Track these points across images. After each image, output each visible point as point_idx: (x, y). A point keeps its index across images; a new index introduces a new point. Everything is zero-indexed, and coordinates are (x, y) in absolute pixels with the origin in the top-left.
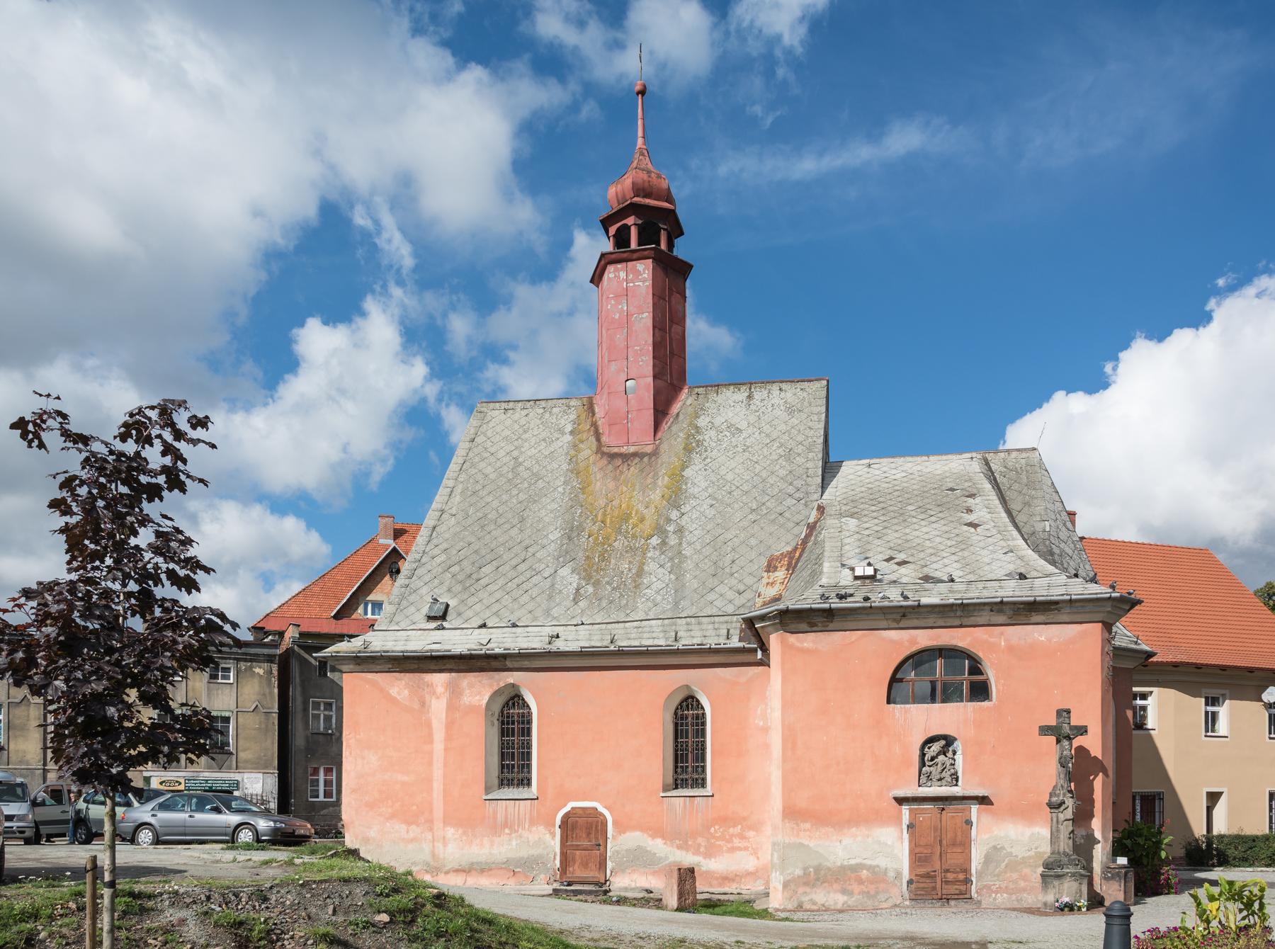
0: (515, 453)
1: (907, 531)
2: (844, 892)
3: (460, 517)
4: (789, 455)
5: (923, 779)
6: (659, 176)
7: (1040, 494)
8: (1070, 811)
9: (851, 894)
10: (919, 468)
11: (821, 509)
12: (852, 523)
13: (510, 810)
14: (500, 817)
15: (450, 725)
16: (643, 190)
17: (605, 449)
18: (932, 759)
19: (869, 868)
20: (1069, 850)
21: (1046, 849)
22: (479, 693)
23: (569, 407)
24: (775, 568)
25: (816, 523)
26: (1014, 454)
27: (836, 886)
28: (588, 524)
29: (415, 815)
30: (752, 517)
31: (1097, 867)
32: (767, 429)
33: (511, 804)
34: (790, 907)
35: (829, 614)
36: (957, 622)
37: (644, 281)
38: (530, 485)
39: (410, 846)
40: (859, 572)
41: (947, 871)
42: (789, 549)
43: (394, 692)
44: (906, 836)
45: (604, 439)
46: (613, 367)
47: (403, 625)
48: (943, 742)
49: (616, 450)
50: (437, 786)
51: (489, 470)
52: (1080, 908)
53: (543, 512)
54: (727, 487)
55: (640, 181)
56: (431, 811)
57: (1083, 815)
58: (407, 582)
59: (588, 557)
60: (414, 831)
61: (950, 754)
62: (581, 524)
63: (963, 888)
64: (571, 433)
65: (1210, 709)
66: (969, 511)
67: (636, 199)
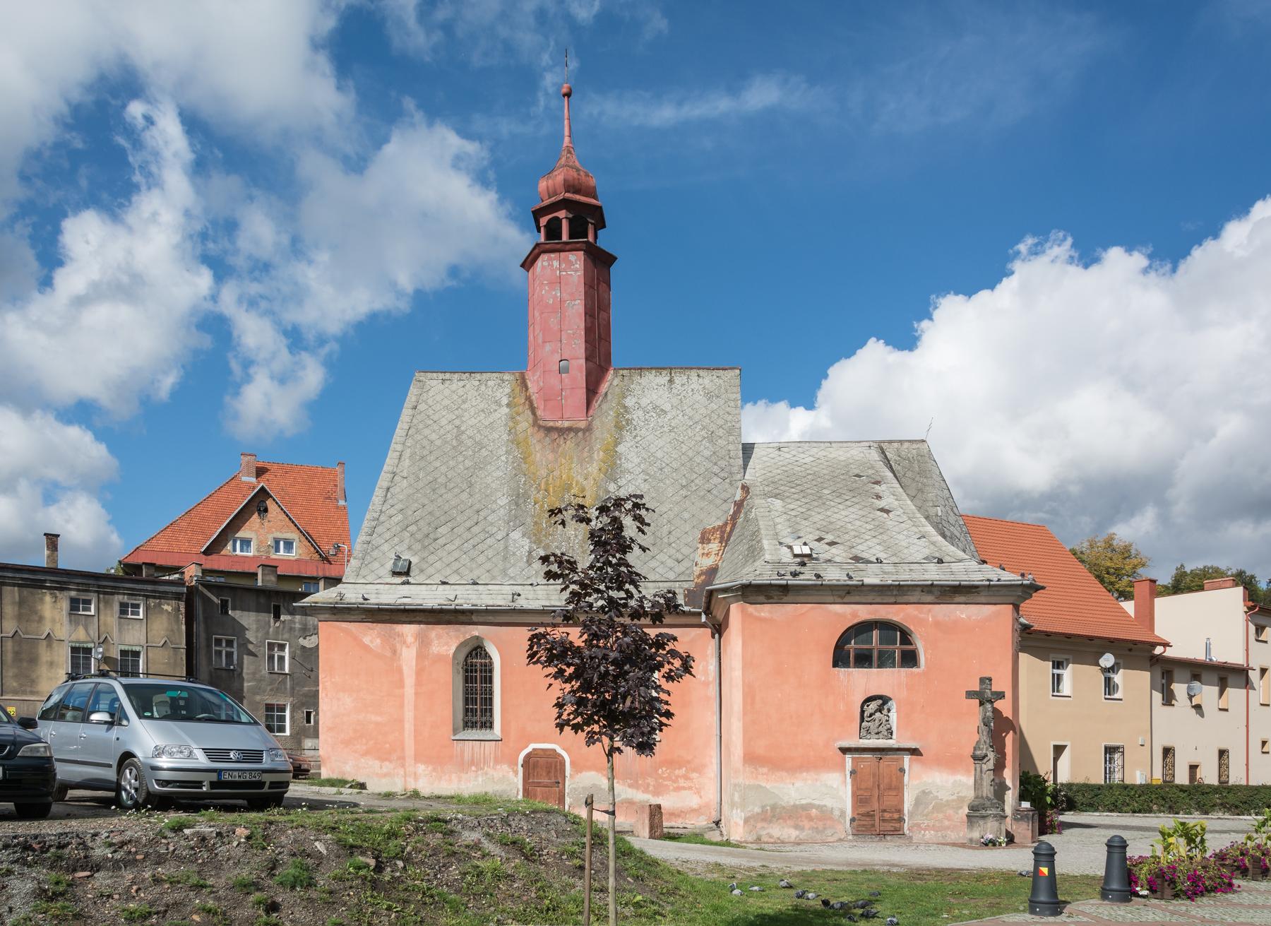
0: (457, 422)
1: (829, 513)
2: (796, 827)
3: (411, 479)
5: (864, 733)
6: (587, 175)
7: (930, 482)
8: (992, 762)
9: (802, 829)
11: (745, 488)
12: (778, 503)
13: (476, 750)
14: (467, 756)
15: (419, 672)
16: (573, 186)
17: (541, 423)
18: (871, 715)
19: (819, 807)
20: (991, 796)
21: (970, 794)
22: (447, 644)
23: (503, 381)
24: (709, 541)
25: (742, 501)
26: (906, 445)
28: (533, 492)
29: (387, 752)
30: (684, 492)
31: (1008, 810)
32: (689, 411)
33: (474, 743)
34: (750, 839)
36: (893, 600)
37: (576, 271)
38: (474, 452)
39: (384, 780)
40: (797, 551)
41: (884, 811)
42: (720, 523)
43: (366, 640)
44: (849, 780)
45: (539, 413)
46: (548, 347)
47: (370, 579)
48: (880, 702)
49: (551, 424)
50: (409, 726)
51: (434, 437)
53: (489, 480)
54: (658, 464)
55: (570, 178)
56: (403, 749)
58: (368, 538)
59: (536, 523)
60: (387, 767)
61: (885, 712)
62: (526, 492)
63: (897, 825)
64: (508, 405)
65: (1056, 671)
66: (879, 497)
67: (568, 195)
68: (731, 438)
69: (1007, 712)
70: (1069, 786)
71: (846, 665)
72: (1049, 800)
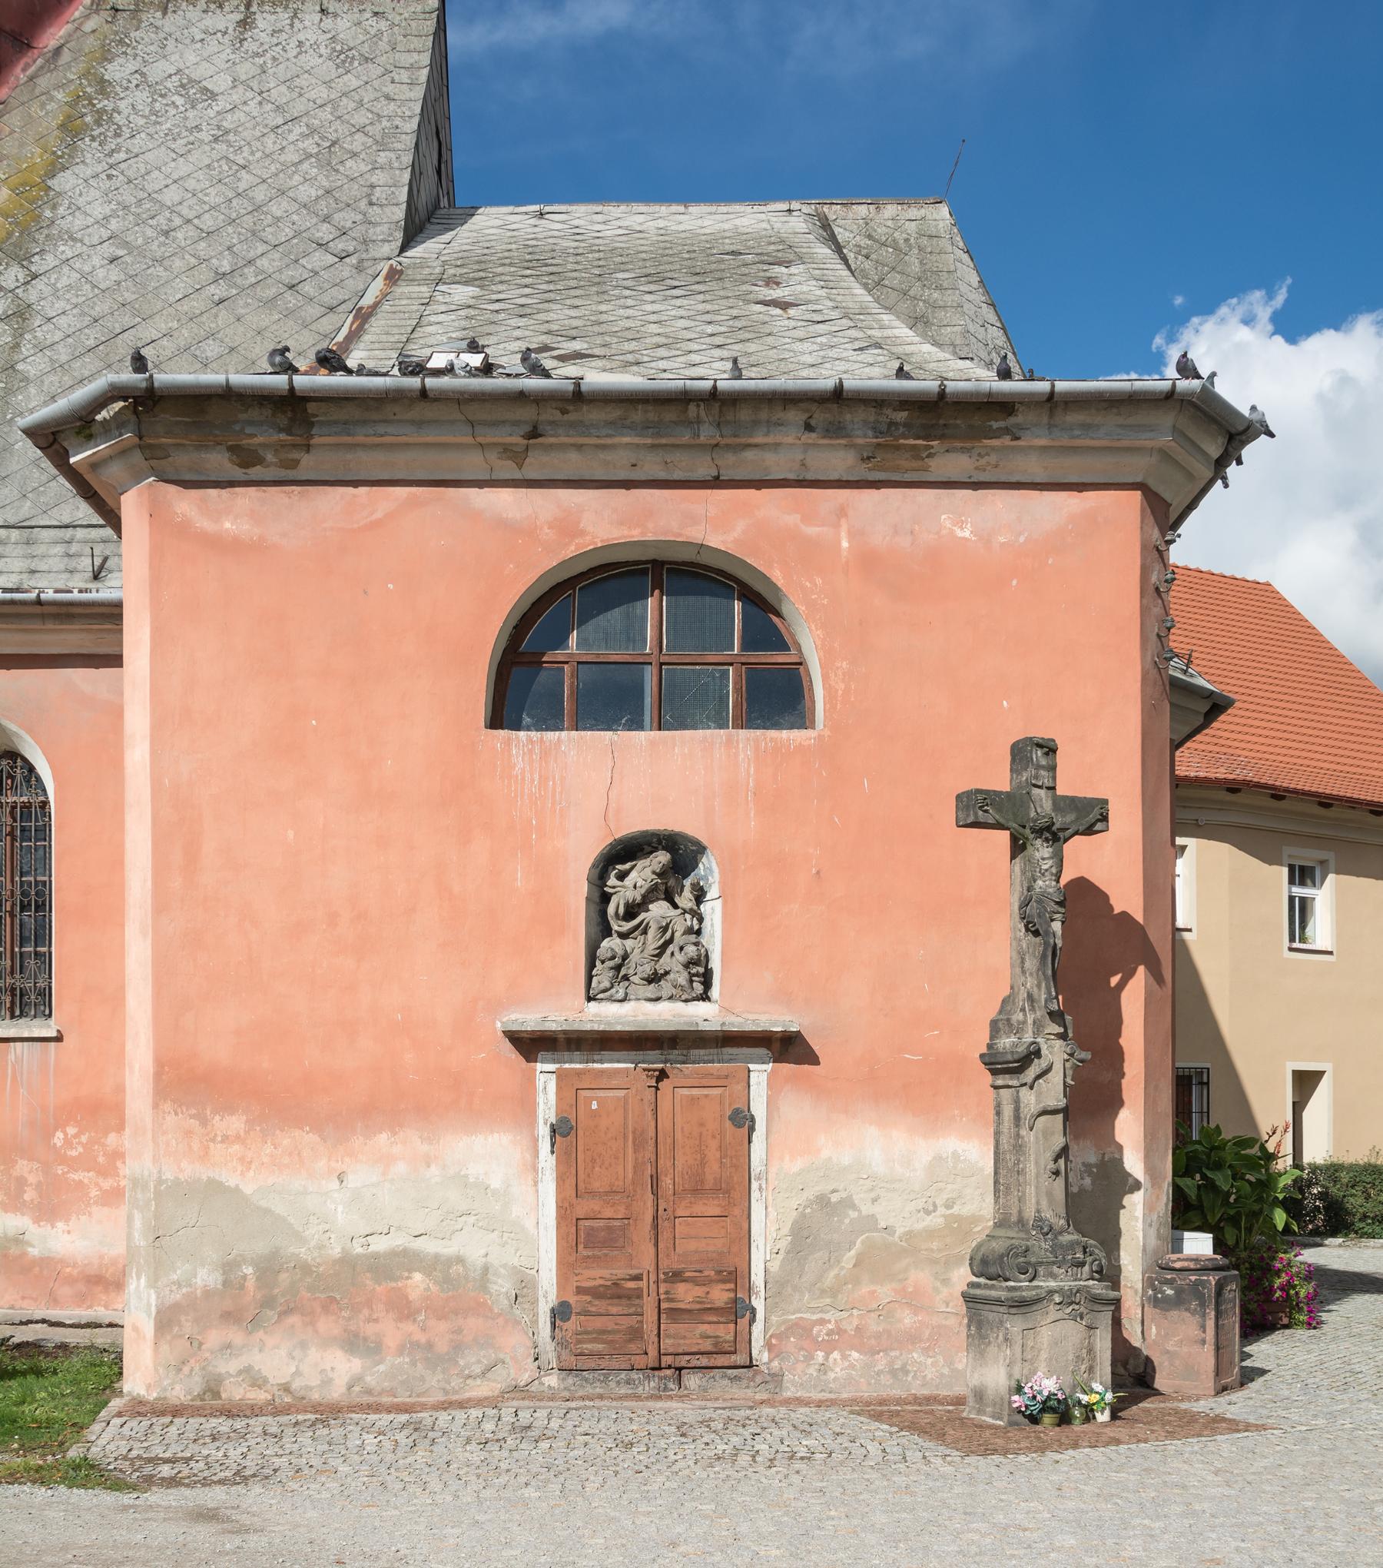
2: (353, 1343)
4: (329, 155)
5: (603, 976)
7: (951, 298)
8: (1056, 1078)
10: (661, 223)
19: (433, 1265)
21: (979, 1206)
27: (327, 1325)
30: (218, 291)
32: (280, 94)
35: (292, 408)
36: (704, 472)
44: (547, 1161)
48: (662, 858)
52: (1089, 1411)
54: (161, 220)
57: (1091, 1102)
61: (686, 900)
63: (725, 1332)
65: (1298, 891)
68: (383, 158)
69: (1127, 897)
70: (1333, 1170)
71: (550, 720)
72: (1280, 1218)
